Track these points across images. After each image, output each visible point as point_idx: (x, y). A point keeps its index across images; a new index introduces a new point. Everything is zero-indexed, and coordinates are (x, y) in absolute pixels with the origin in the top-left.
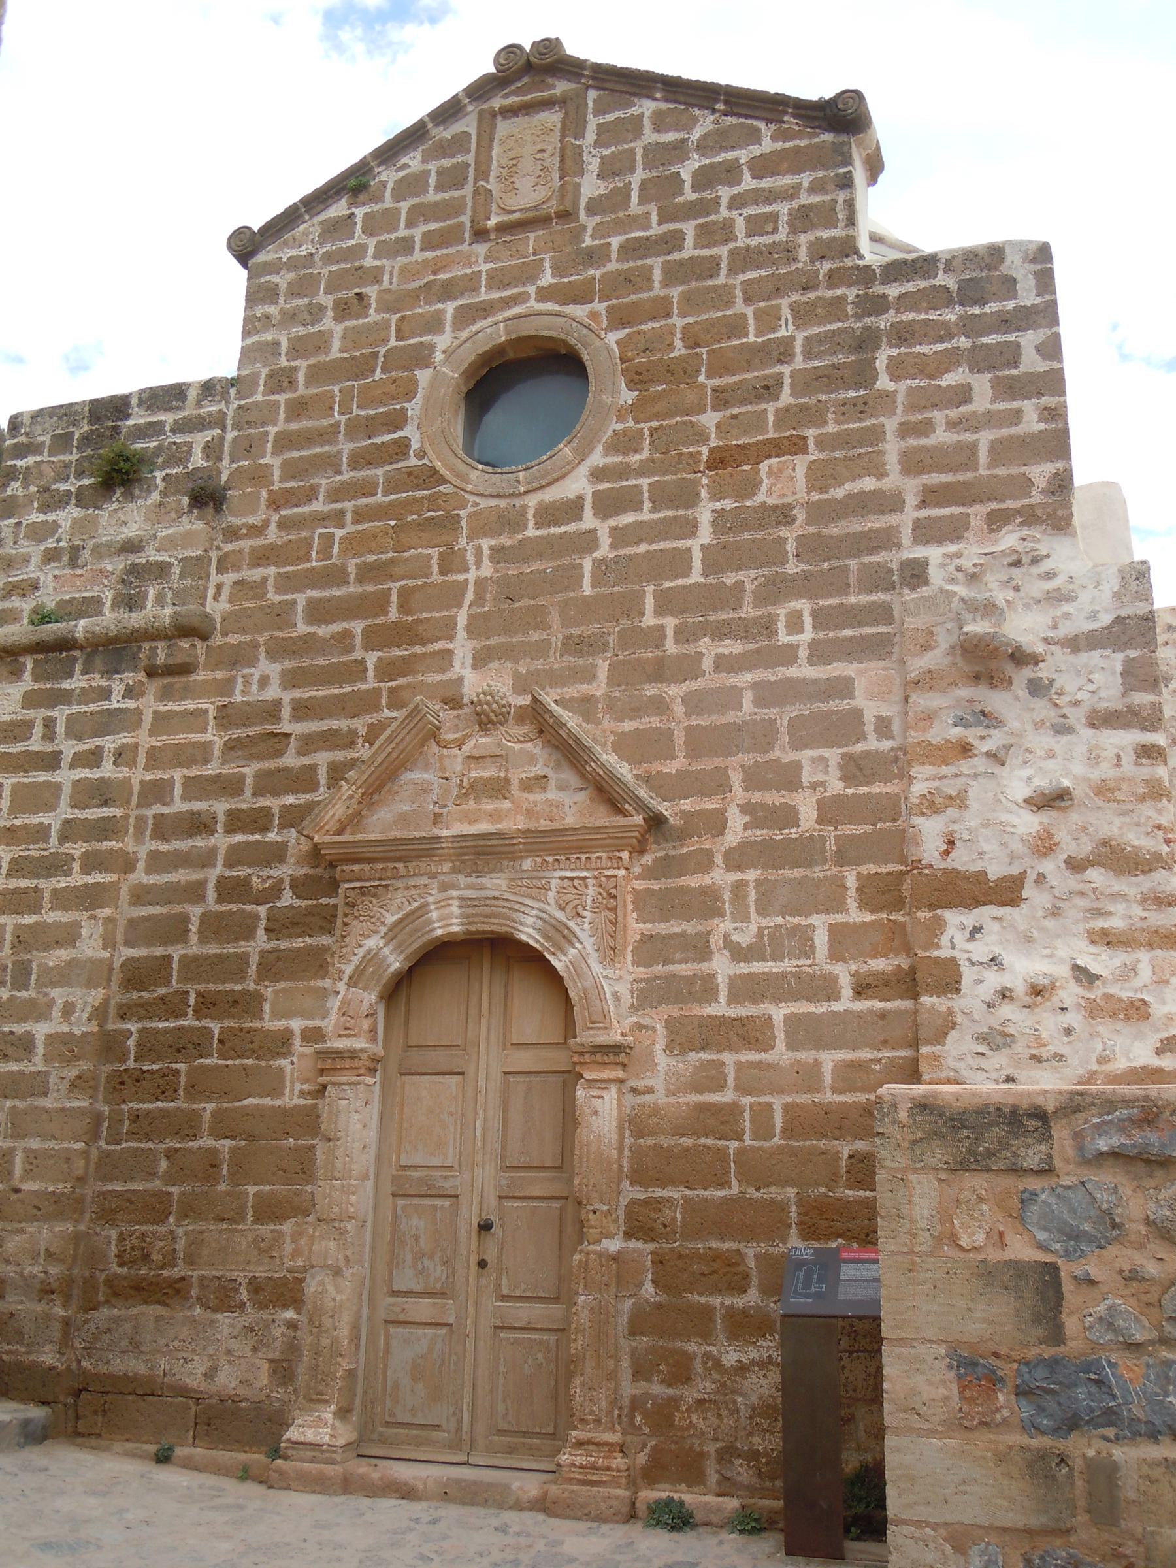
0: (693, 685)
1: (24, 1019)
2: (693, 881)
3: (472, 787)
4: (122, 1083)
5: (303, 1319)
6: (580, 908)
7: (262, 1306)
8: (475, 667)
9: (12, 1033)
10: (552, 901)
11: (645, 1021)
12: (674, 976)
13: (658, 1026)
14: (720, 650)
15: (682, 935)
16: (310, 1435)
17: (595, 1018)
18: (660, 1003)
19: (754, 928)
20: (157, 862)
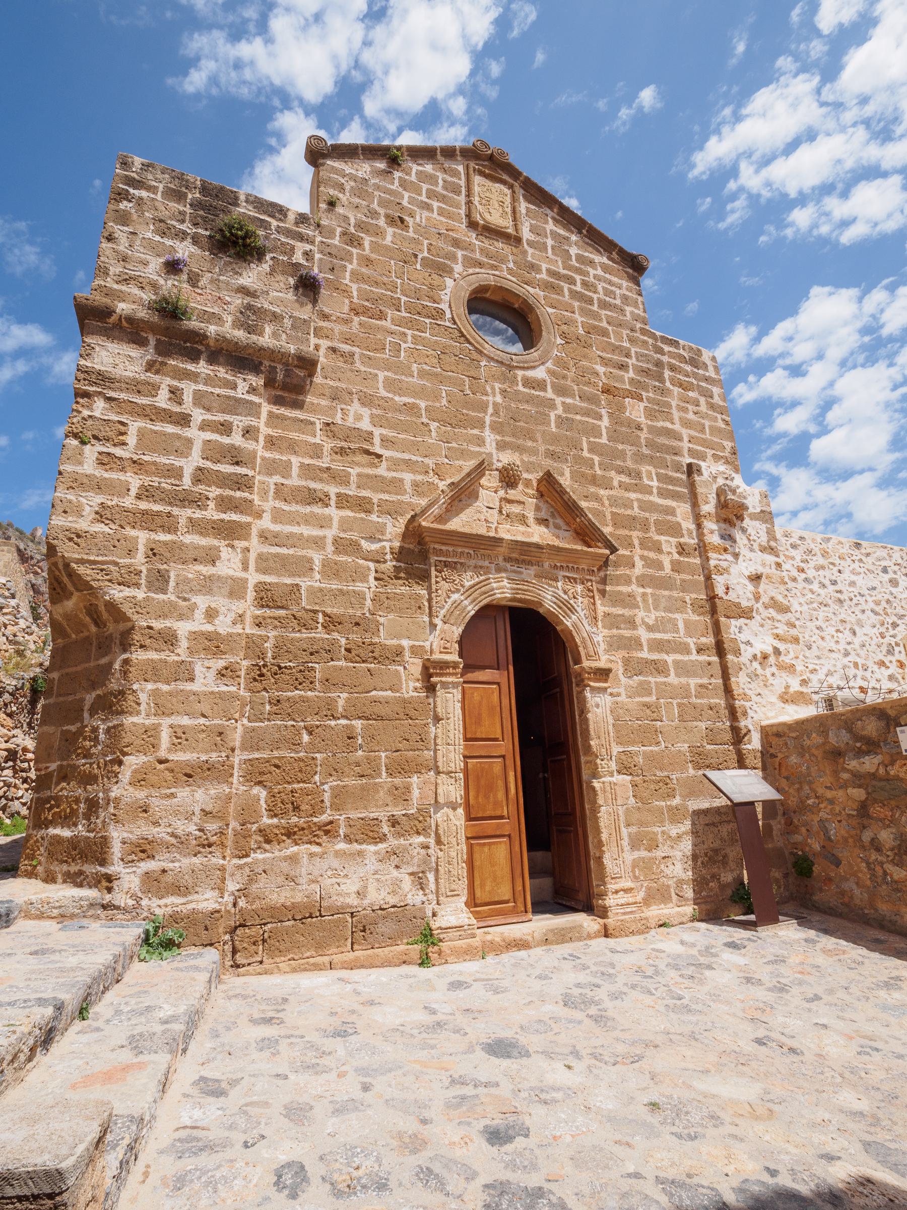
1: (165, 616)
2: (624, 589)
4: (262, 675)
5: (432, 841)
7: (400, 835)
9: (150, 628)
11: (612, 658)
15: (623, 615)
16: (452, 921)
19: (653, 617)
20: (278, 515)
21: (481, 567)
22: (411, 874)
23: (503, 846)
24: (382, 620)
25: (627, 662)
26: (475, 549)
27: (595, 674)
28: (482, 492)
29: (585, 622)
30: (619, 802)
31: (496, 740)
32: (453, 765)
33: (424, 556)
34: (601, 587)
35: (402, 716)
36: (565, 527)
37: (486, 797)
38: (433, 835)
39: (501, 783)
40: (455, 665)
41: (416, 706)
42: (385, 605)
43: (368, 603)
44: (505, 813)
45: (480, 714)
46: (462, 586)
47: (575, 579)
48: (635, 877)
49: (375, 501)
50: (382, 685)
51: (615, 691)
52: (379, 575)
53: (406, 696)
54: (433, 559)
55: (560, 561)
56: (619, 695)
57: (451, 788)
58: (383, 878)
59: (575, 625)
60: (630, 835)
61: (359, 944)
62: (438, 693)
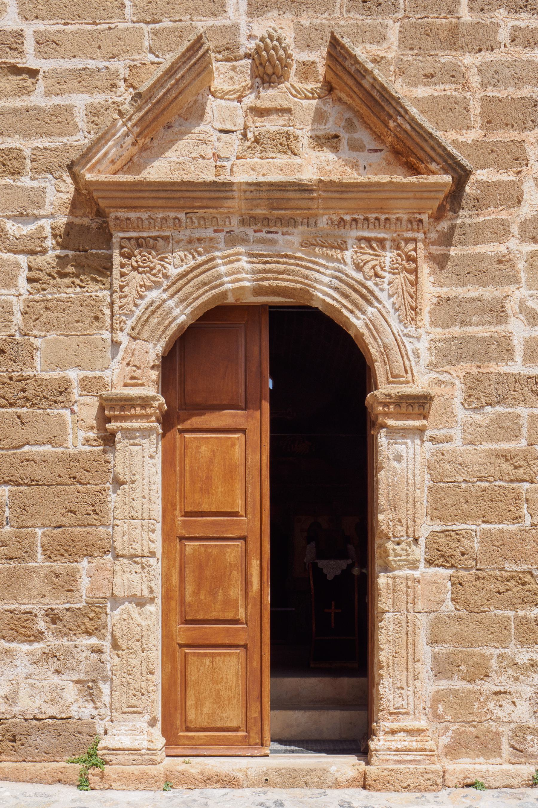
0: (487, 56)
3: (257, 141)
5: (107, 644)
6: (378, 269)
7: (62, 634)
8: (250, 14)
10: (349, 260)
12: (472, 337)
13: (457, 382)
14: (517, 23)
16: (126, 742)
17: (396, 372)
18: (458, 361)
21: (199, 240)
22: (77, 682)
23: (234, 659)
24: (38, 342)
25: (472, 384)
26: (189, 209)
27: (398, 405)
28: (213, 106)
29: (393, 320)
30: (419, 607)
31: (235, 514)
32: (137, 546)
33: (105, 237)
34: (436, 250)
35: (66, 479)
36: (373, 145)
37: (212, 593)
38: (109, 636)
39: (237, 576)
40: (145, 402)
41: (87, 465)
42: (43, 319)
43: (17, 318)
44: (241, 615)
45: (209, 478)
46: (166, 276)
47: (381, 242)
48: (436, 715)
49: (27, 153)
50: (38, 437)
51: (440, 433)
52: (34, 274)
53: (72, 451)
54: (118, 236)
55: (350, 211)
56: (448, 439)
57: (134, 577)
58: (39, 684)
59: (372, 325)
60: (435, 657)
61: (7, 755)
62: (118, 446)
